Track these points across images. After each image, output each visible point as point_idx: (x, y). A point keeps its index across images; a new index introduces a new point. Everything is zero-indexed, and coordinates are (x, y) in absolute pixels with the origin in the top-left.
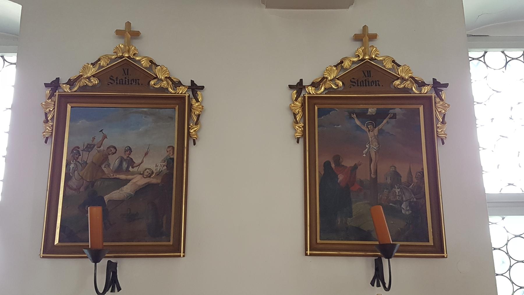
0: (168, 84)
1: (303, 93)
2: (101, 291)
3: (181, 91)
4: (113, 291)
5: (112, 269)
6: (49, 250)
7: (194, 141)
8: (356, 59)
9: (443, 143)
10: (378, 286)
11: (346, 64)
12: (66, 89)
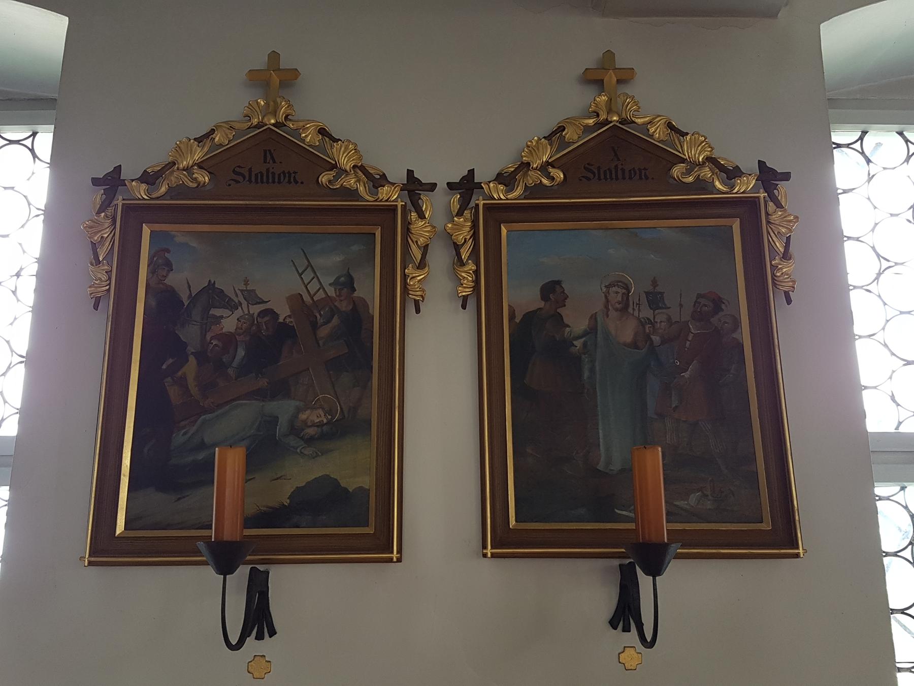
0: (359, 181)
3: (389, 194)
4: (260, 637)
6: (106, 548)
8: (591, 122)
9: (789, 301)
10: (626, 629)
11: (569, 134)
12: (141, 191)
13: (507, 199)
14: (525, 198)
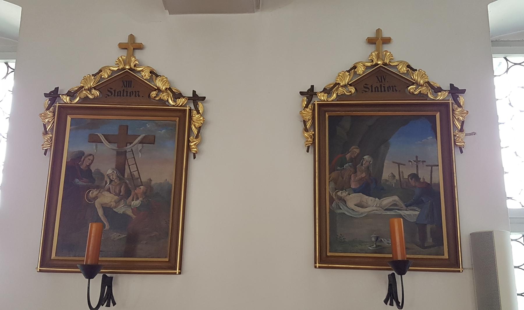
1: (313, 99)
2: (94, 307)
5: (107, 283)
7: (194, 154)
8: (369, 64)
9: (462, 152)
10: (391, 304)
11: (360, 70)
13: (327, 101)
14: (337, 101)
